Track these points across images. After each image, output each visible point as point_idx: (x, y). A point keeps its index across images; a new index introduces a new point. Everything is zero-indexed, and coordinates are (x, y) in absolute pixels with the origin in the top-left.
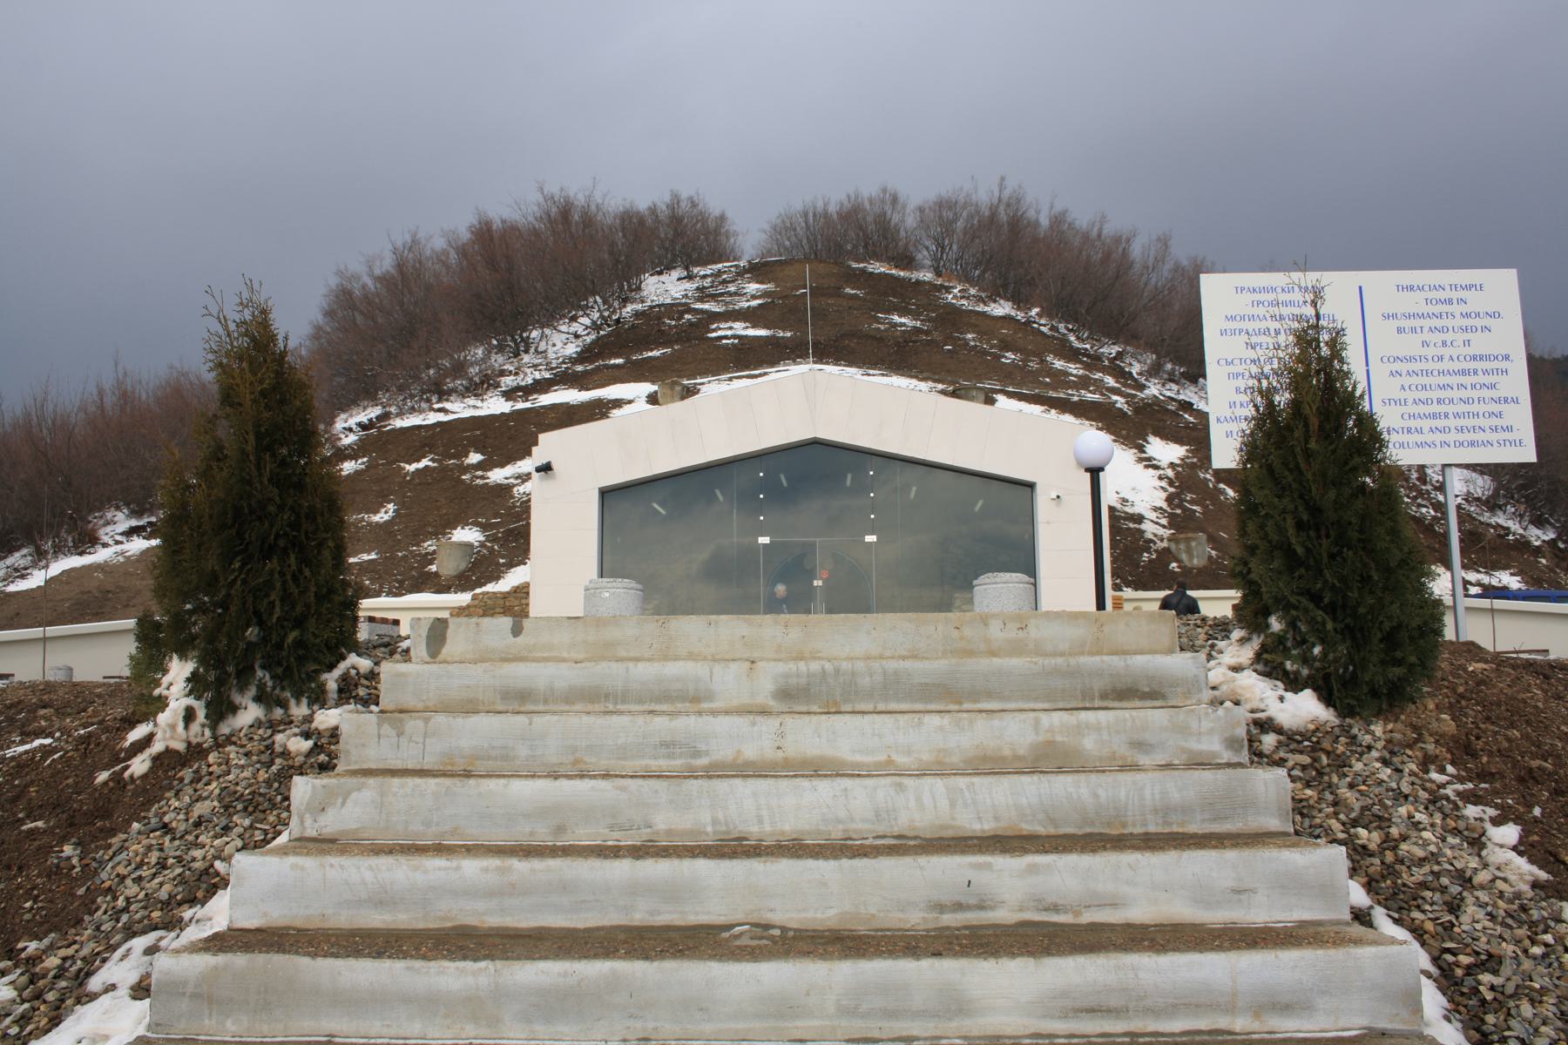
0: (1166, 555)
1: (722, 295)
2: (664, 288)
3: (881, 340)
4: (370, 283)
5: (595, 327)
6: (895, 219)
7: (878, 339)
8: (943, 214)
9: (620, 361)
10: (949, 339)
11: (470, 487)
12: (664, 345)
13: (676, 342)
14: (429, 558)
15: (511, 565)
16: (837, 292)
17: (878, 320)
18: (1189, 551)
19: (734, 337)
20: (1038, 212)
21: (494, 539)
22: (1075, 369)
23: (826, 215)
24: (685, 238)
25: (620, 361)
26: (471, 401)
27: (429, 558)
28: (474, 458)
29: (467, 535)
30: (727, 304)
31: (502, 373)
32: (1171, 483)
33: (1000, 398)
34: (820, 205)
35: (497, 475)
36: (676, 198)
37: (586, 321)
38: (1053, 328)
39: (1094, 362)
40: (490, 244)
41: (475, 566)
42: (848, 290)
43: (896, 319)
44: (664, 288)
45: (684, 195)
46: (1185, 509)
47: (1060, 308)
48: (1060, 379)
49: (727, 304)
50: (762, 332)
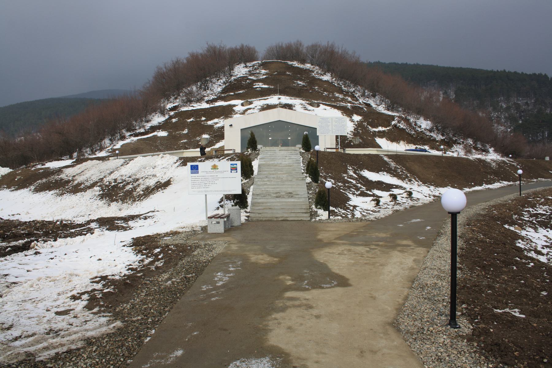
0: (351, 141)
1: (255, 74)
2: (240, 71)
3: (294, 89)
4: (165, 70)
5: (224, 83)
6: (301, 48)
7: (294, 89)
8: (314, 48)
9: (232, 94)
10: (311, 88)
11: (204, 125)
12: (243, 89)
13: (246, 88)
14: (199, 141)
15: (217, 142)
16: (284, 74)
17: (294, 83)
18: (355, 141)
19: (260, 88)
20: (339, 49)
21: (212, 137)
22: (341, 96)
23: (282, 46)
24: (245, 55)
25: (232, 94)
26: (199, 104)
27: (199, 141)
28: (203, 119)
29: (205, 136)
30: (257, 77)
31: (204, 96)
32: (356, 125)
33: (321, 105)
34: (280, 44)
35: (210, 123)
36: (243, 46)
37: (222, 81)
38: (338, 84)
39: (347, 94)
40: (194, 59)
41: (209, 143)
42: (288, 73)
43: (299, 82)
44: (240, 71)
45: (245, 45)
46: (358, 131)
47: (341, 76)
48: (337, 99)
49: (257, 77)
50: (266, 86)
